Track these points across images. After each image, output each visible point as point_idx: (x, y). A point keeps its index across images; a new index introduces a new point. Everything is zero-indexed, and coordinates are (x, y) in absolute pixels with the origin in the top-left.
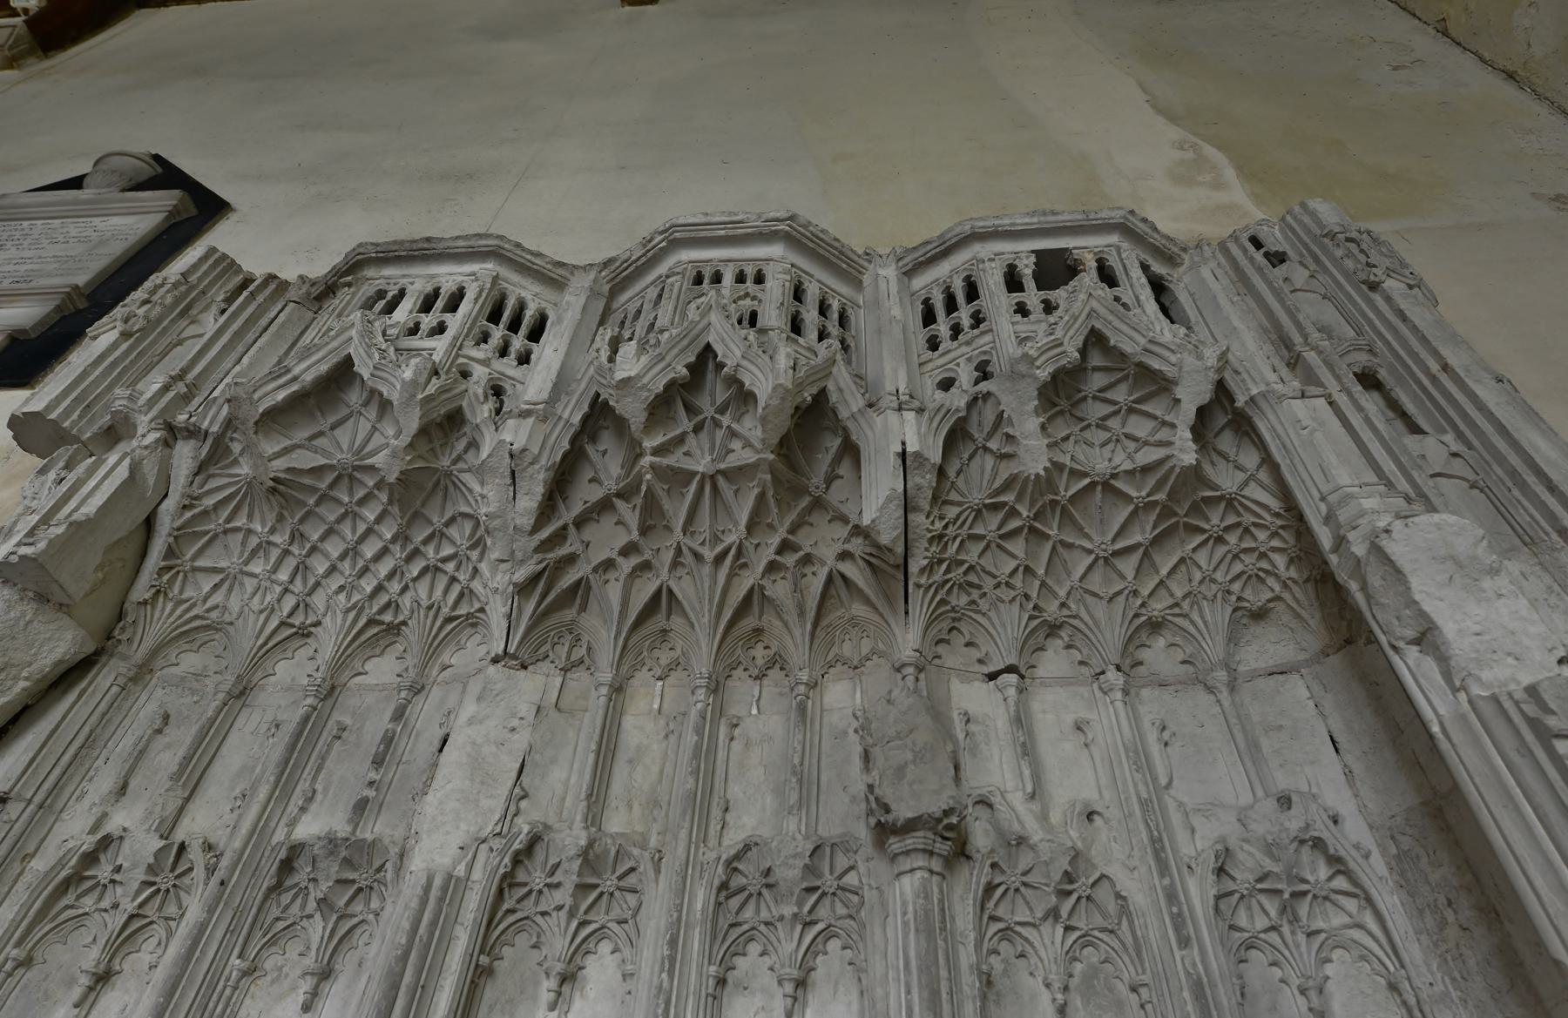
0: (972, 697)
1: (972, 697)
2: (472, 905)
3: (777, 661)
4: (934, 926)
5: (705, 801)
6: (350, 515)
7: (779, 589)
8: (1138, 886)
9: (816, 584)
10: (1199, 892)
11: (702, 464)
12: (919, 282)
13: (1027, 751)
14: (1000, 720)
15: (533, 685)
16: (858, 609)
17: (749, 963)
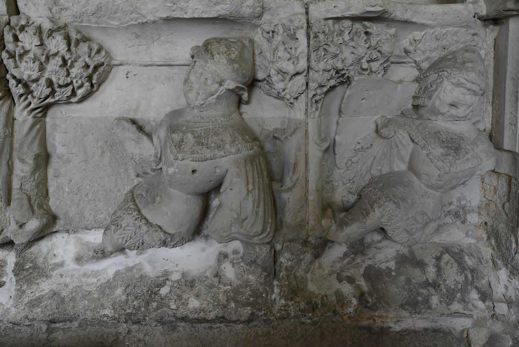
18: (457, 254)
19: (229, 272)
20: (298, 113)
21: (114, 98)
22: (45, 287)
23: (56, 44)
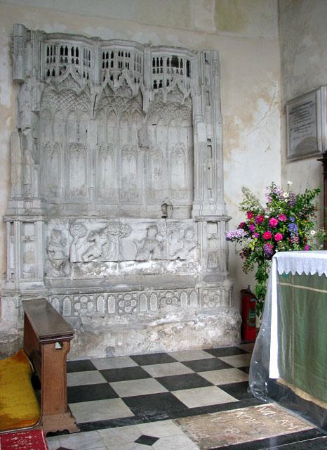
0: (151, 128)
1: (151, 128)
2: (97, 152)
3: (127, 120)
4: (145, 156)
5: (119, 141)
6: (67, 95)
7: (128, 111)
8: (164, 151)
9: (133, 110)
10: (170, 152)
11: (122, 96)
12: (153, 53)
13: (156, 136)
14: (153, 131)
15: (96, 123)
16: (138, 114)
17: (125, 158)
18: (192, 263)
19: (154, 266)
20: (165, 238)
21: (132, 236)
22: (122, 270)
23: (127, 227)
